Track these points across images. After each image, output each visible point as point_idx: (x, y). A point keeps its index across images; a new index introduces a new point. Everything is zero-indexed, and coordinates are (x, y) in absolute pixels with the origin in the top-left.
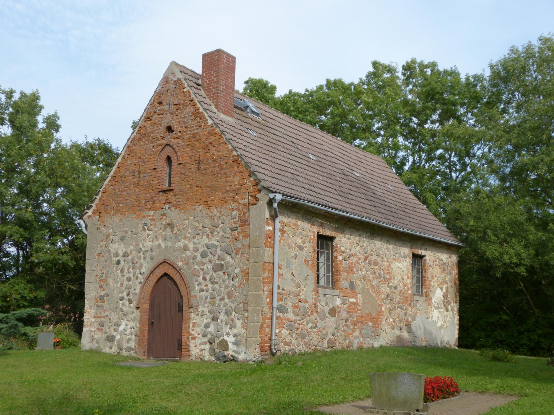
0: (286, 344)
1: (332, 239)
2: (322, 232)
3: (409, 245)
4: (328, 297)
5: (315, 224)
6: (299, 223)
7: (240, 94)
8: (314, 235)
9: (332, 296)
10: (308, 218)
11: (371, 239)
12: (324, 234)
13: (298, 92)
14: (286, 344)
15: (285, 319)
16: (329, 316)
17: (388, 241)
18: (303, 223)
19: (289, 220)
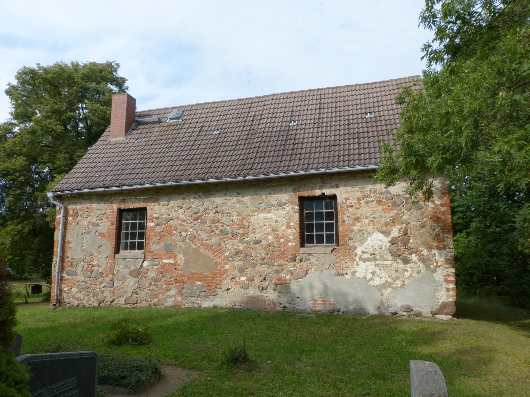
0: (75, 299)
1: (145, 209)
2: (123, 206)
3: (291, 189)
4: (129, 261)
5: (114, 202)
6: (94, 205)
7: (430, 318)
8: (113, 212)
9: (134, 260)
10: (104, 200)
11: (205, 198)
12: (311, 195)
13: (58, 65)
14: (75, 299)
15: (74, 280)
16: (130, 277)
17: (238, 194)
18: (98, 205)
19: (82, 206)
